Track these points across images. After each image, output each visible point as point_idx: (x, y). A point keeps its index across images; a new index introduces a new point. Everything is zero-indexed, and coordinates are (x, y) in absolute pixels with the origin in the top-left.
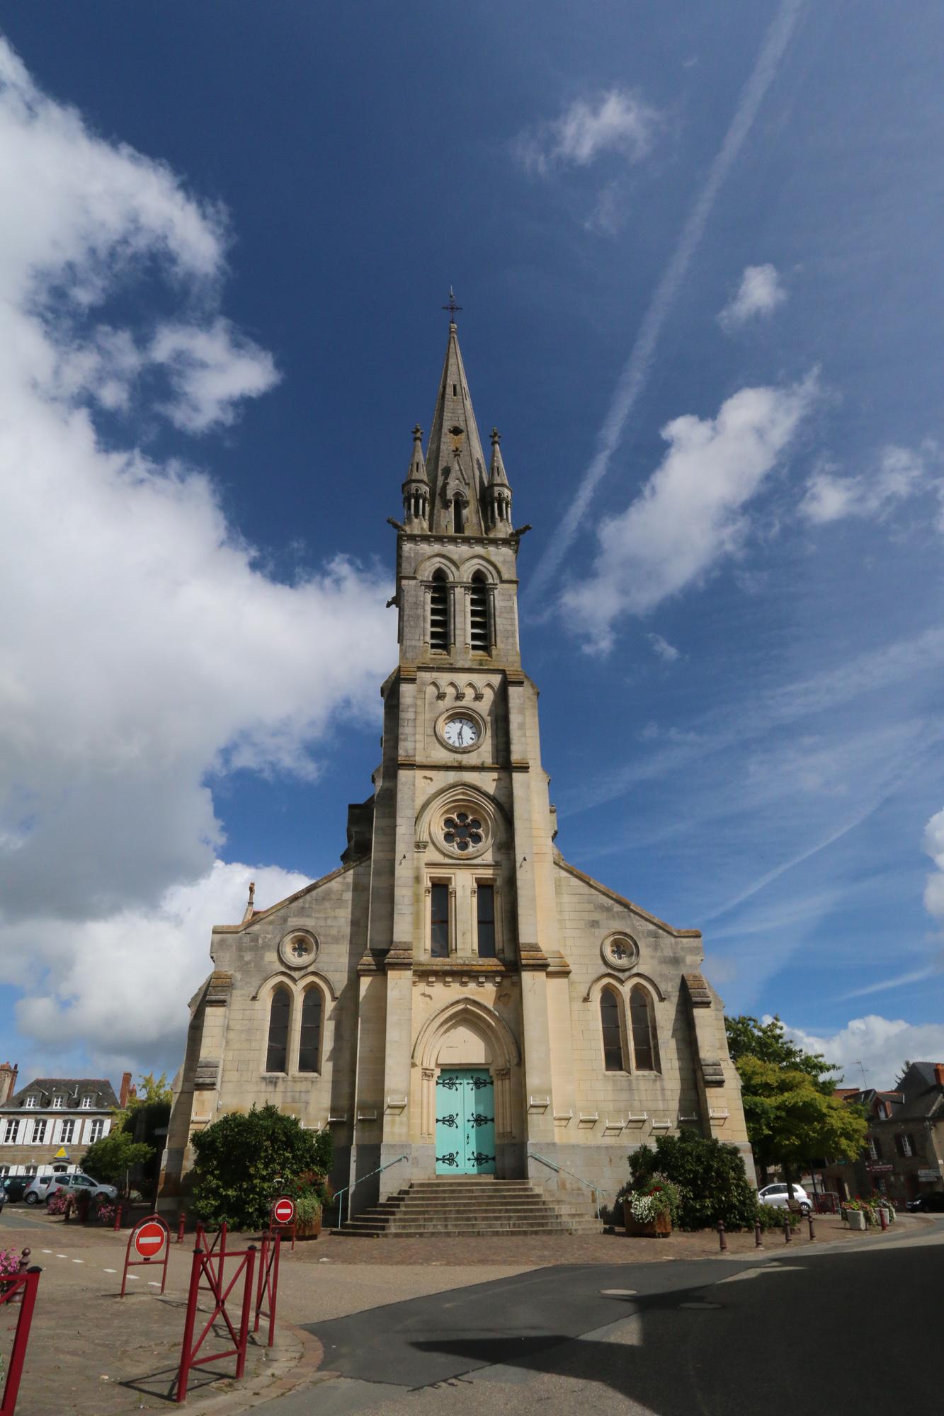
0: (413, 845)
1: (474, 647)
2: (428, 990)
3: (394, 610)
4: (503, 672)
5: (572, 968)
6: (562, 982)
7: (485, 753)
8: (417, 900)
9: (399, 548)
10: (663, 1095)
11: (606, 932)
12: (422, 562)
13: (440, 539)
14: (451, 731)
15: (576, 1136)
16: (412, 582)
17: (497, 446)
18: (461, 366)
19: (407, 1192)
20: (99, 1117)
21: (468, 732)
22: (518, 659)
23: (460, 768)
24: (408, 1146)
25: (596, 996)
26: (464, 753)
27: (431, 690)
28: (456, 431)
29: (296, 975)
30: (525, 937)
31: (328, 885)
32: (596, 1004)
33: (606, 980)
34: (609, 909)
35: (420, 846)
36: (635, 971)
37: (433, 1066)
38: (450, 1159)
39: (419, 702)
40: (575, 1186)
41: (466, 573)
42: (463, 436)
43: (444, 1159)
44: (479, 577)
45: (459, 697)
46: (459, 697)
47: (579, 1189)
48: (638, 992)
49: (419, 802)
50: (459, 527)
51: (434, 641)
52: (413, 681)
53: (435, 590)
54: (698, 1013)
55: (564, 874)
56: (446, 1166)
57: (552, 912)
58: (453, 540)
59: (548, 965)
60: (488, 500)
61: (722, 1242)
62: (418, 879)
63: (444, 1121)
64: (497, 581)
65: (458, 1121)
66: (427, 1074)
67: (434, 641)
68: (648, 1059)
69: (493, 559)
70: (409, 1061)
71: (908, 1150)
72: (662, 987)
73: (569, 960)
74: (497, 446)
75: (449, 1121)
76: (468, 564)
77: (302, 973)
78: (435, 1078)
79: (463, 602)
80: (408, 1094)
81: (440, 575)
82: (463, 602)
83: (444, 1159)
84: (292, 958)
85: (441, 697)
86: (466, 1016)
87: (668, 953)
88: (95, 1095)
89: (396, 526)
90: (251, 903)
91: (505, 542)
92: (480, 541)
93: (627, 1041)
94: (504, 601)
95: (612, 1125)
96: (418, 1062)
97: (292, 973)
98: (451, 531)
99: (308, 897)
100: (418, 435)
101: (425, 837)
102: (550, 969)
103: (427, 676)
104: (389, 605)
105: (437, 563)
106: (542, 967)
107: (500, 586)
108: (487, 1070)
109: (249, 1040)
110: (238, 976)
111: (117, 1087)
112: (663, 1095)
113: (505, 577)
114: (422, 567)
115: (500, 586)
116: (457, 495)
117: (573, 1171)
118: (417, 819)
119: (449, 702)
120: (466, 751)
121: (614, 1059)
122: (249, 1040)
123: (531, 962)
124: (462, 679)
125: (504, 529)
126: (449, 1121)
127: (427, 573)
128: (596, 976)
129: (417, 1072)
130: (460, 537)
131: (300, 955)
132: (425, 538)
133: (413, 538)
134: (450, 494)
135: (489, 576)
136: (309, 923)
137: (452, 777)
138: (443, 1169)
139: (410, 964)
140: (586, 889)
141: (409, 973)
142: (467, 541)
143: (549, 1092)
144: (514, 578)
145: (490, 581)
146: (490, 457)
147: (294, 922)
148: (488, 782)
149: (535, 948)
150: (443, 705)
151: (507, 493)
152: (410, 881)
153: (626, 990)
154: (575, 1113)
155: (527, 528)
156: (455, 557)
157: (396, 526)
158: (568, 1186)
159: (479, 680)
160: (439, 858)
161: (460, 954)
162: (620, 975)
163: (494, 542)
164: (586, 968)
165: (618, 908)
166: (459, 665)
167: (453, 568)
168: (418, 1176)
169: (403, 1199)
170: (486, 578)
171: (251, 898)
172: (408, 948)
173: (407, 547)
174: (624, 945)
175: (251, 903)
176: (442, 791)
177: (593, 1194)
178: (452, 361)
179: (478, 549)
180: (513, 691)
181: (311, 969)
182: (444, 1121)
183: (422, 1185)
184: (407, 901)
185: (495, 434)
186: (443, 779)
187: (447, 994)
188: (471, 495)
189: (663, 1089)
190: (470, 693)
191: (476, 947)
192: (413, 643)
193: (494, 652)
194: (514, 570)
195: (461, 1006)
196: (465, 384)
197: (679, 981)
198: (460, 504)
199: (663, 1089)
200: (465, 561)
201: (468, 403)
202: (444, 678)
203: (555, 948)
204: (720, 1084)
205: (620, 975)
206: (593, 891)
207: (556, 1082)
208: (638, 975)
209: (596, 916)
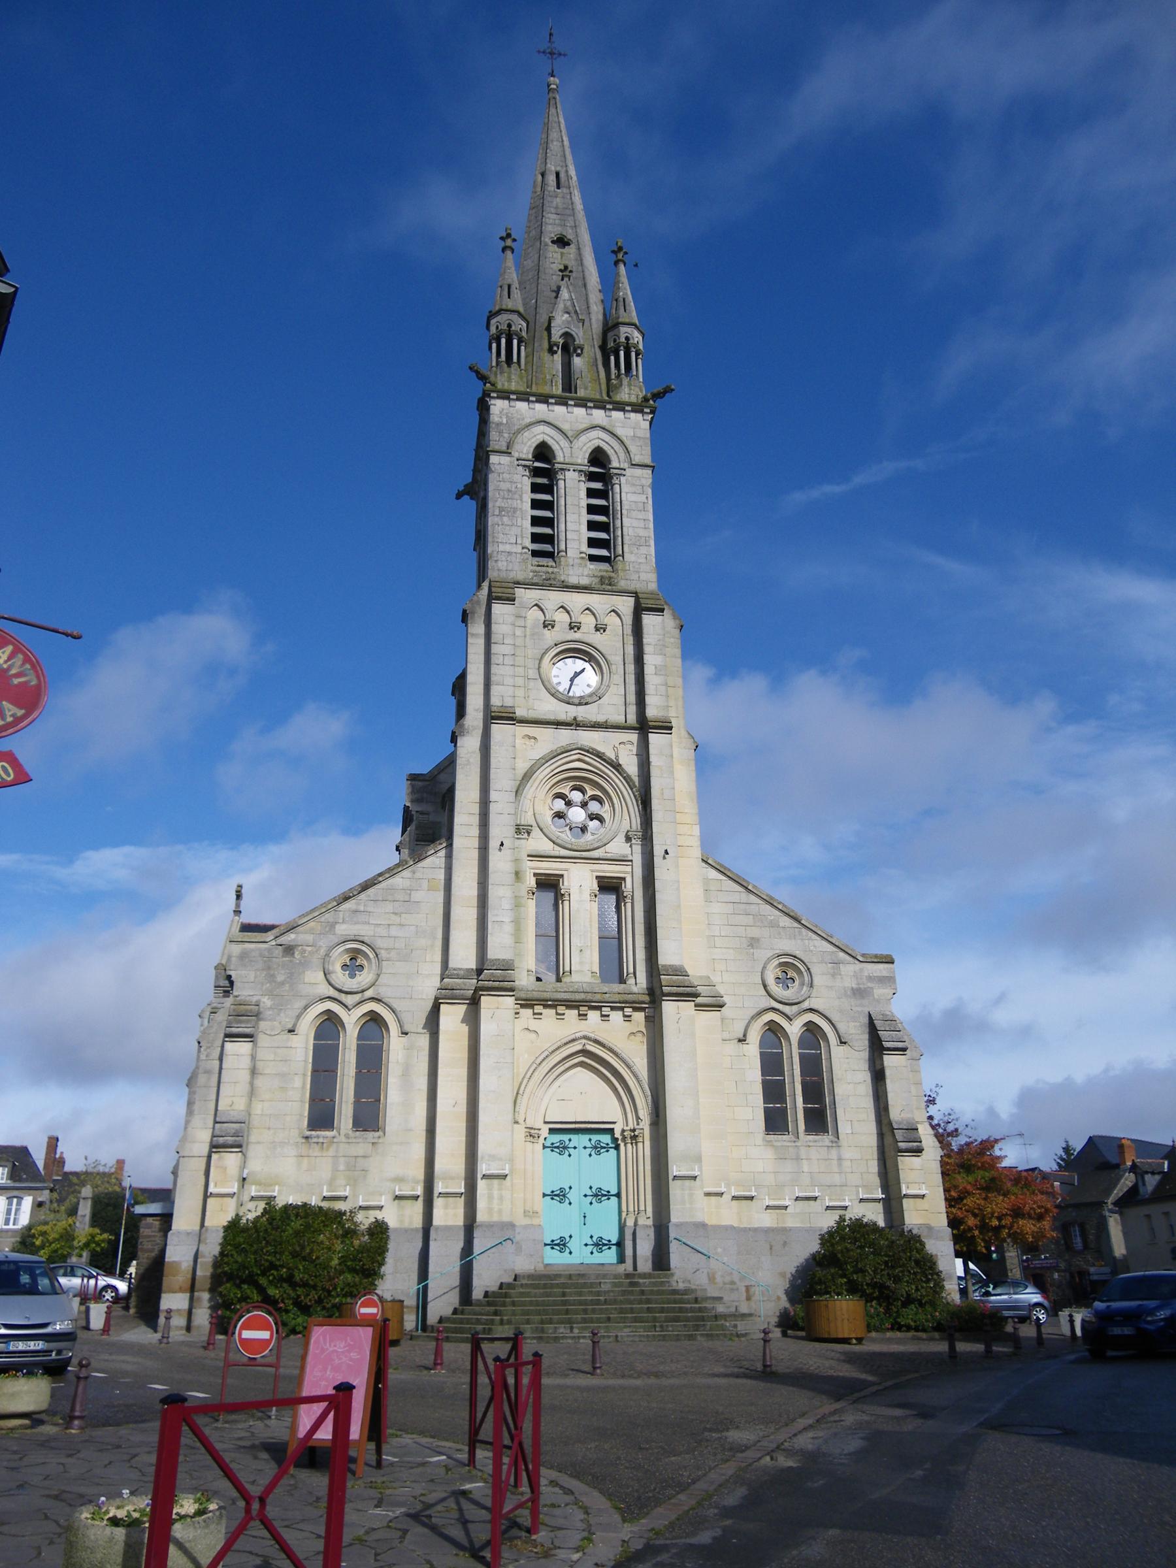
0: (513, 829)
1: (592, 558)
2: (534, 1024)
3: (469, 505)
4: (636, 595)
5: (726, 999)
6: (713, 1016)
7: (615, 705)
8: (517, 905)
9: (483, 407)
10: (840, 1165)
11: (770, 954)
12: (519, 431)
13: (544, 399)
14: (561, 672)
15: (726, 1214)
16: (505, 459)
17: (622, 267)
18: (566, 143)
19: (510, 1286)
20: (16, 1193)
21: (590, 678)
22: (653, 577)
23: (575, 724)
24: (511, 1225)
25: (755, 1036)
26: (580, 704)
27: (535, 614)
28: (562, 242)
29: (350, 1000)
30: (667, 955)
31: (390, 881)
32: (753, 1050)
33: (771, 1016)
34: (773, 925)
35: (522, 830)
36: (806, 1005)
37: (539, 1124)
38: (561, 1244)
39: (519, 632)
40: (728, 1279)
41: (580, 453)
42: (571, 250)
43: (552, 1245)
44: (598, 457)
45: (574, 626)
46: (574, 626)
47: (733, 1283)
48: (812, 1033)
49: (522, 766)
50: (569, 384)
51: (536, 547)
52: (511, 600)
53: (536, 472)
54: (891, 1062)
55: (713, 874)
56: (555, 1253)
57: (699, 928)
58: (562, 402)
59: (696, 995)
60: (610, 348)
61: (438, 1352)
62: (518, 875)
63: (553, 1195)
64: (626, 465)
65: (572, 1196)
66: (532, 1134)
67: (536, 547)
68: (819, 1119)
69: (620, 432)
70: (510, 1116)
71: (1078, 1243)
72: (842, 1027)
73: (721, 989)
74: (622, 267)
75: (559, 1195)
76: (583, 438)
77: (357, 997)
78: (541, 1140)
79: (573, 493)
80: (511, 1160)
81: (543, 452)
82: (573, 493)
83: (552, 1245)
84: (341, 978)
85: (548, 625)
86: (593, 1059)
87: (850, 983)
88: (10, 1165)
89: (483, 378)
90: (237, 912)
91: (637, 408)
92: (600, 405)
93: (796, 1097)
94: (634, 495)
95: (772, 1203)
96: (521, 1121)
97: (342, 997)
98: (558, 390)
99: (363, 896)
100: (509, 242)
101: (528, 819)
102: (699, 1000)
103: (531, 595)
104: (459, 496)
105: (541, 434)
106: (688, 994)
107: (629, 472)
108: (611, 1131)
109: (283, 1089)
110: (266, 1002)
111: (39, 1157)
112: (840, 1165)
113: (637, 459)
114: (519, 438)
115: (629, 472)
116: (567, 335)
117: (725, 1259)
118: (518, 792)
119: (560, 633)
120: (582, 702)
121: (775, 1122)
122: (283, 1089)
123: (674, 990)
124: (577, 601)
125: (630, 392)
126: (559, 1195)
127: (525, 447)
128: (755, 1012)
129: (520, 1131)
130: (569, 393)
131: (352, 976)
132: (523, 397)
133: (505, 395)
134: (556, 335)
135: (613, 457)
136: (365, 931)
137: (566, 737)
138: (554, 1258)
139: (512, 990)
140: (744, 896)
141: (509, 1001)
142: (582, 403)
143: (698, 1159)
144: (648, 461)
145: (615, 464)
146: (609, 285)
147: (343, 930)
148: (622, 748)
149: (679, 971)
150: (550, 636)
151: (637, 337)
152: (510, 878)
153: (794, 1030)
154: (728, 1186)
155: (668, 390)
156: (565, 427)
157: (483, 378)
158: (719, 1279)
159: (597, 601)
160: (546, 847)
161: (575, 977)
162: (786, 1009)
163: (620, 406)
164: (744, 998)
165: (786, 921)
166: (573, 580)
167: (564, 443)
168: (523, 1264)
169: (506, 1295)
170: (610, 462)
171: (238, 905)
172: (507, 966)
173: (498, 407)
174: (790, 969)
175: (237, 912)
176: (554, 755)
177: (748, 1288)
178: (554, 135)
179: (598, 415)
180: (648, 620)
181: (368, 994)
182: (553, 1195)
183: (530, 1276)
184: (506, 904)
185: (620, 249)
186: (550, 739)
187: (558, 1028)
188: (588, 336)
189: (840, 1159)
190: (588, 621)
191: (596, 969)
192: (508, 548)
193: (620, 566)
194: (647, 450)
195: (577, 1047)
196: (572, 173)
197: (866, 1020)
198: (569, 348)
199: (840, 1159)
200: (574, 431)
201: (577, 198)
202: (552, 599)
203: (704, 974)
204: (918, 1151)
205: (786, 1009)
206: (753, 898)
207: (707, 1148)
208: (811, 1010)
209: (754, 932)
